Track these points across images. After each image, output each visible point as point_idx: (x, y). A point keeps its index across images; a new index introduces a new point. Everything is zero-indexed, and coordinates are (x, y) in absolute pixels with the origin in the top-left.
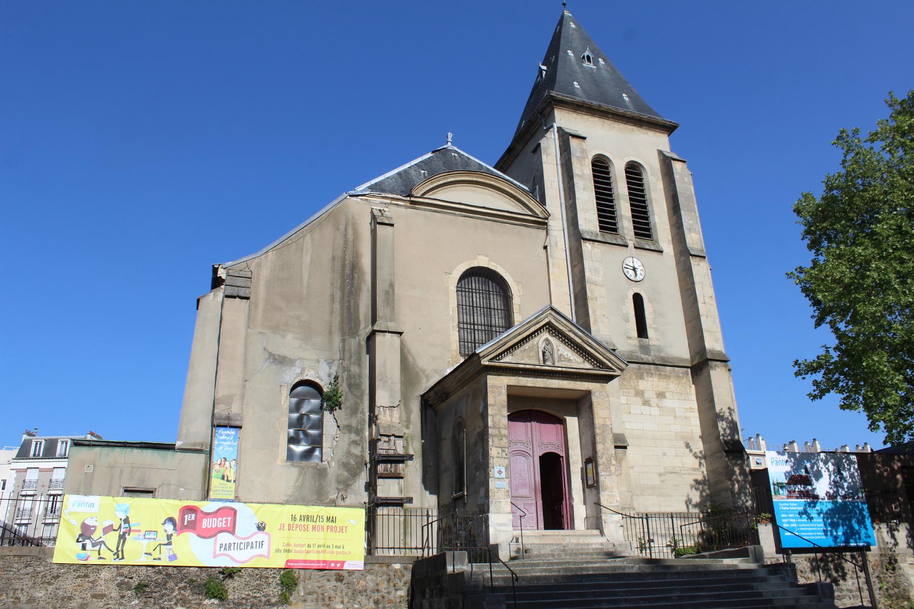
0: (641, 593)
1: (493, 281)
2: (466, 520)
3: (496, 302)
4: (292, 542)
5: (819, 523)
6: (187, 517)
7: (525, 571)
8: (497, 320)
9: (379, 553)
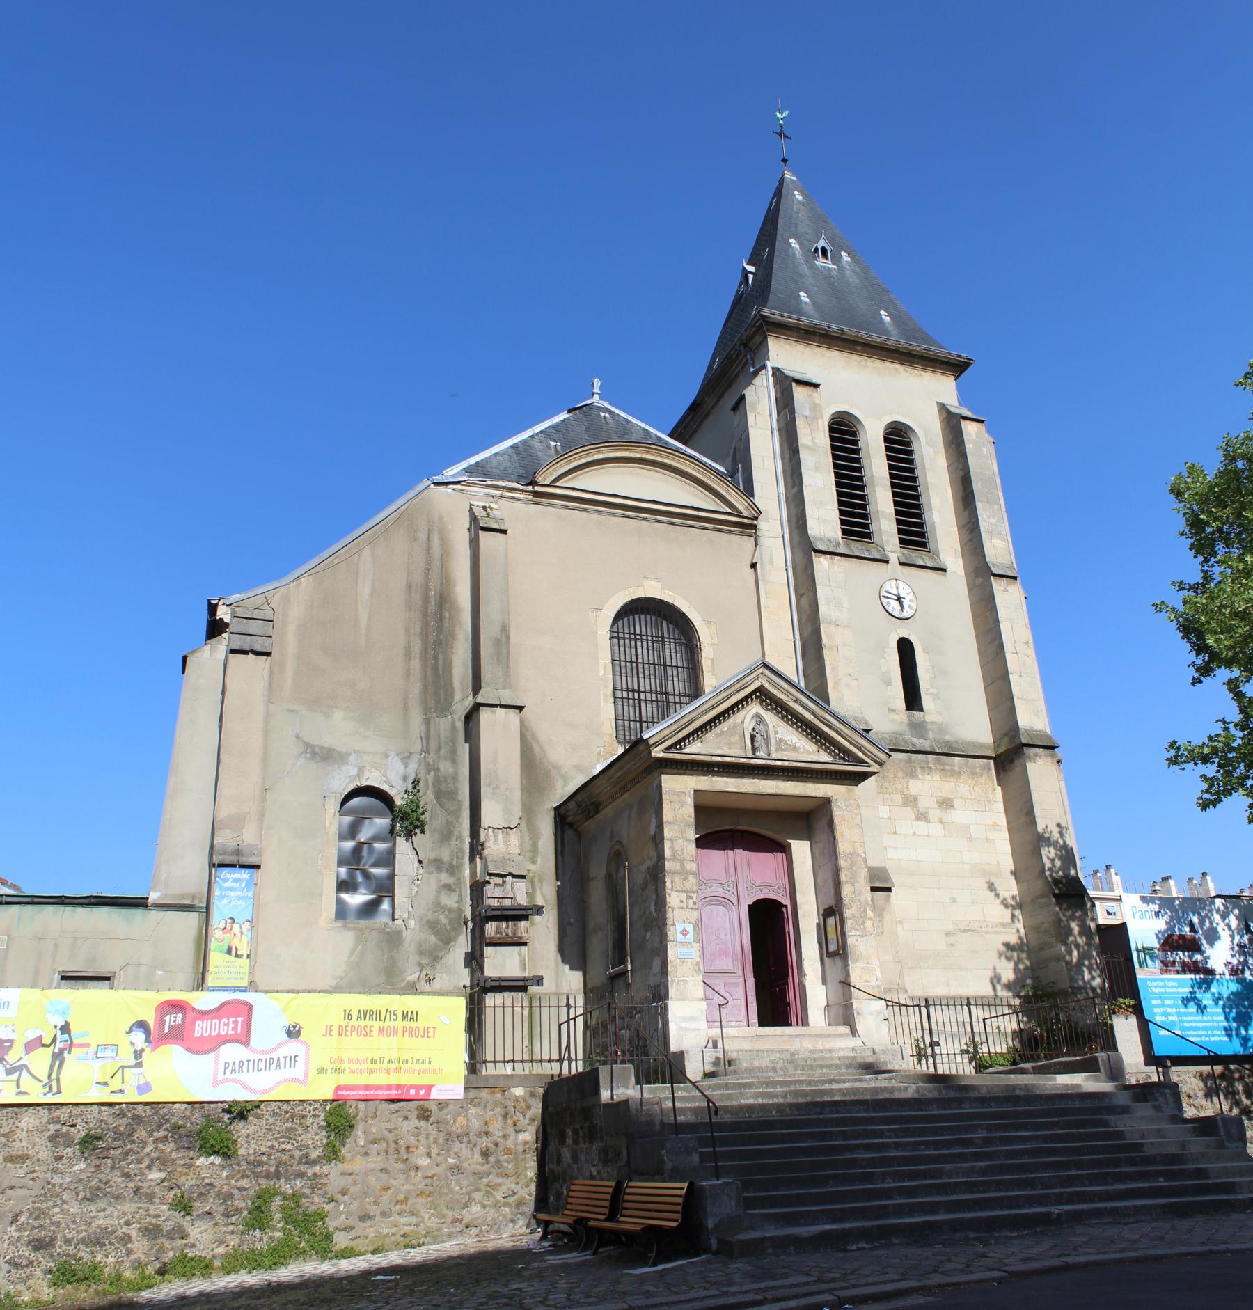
0: (922, 1132)
1: (670, 621)
2: (631, 1012)
3: (674, 655)
4: (345, 1055)
5: (1217, 1014)
6: (169, 1020)
7: (730, 1097)
8: (677, 684)
9: (488, 1070)
